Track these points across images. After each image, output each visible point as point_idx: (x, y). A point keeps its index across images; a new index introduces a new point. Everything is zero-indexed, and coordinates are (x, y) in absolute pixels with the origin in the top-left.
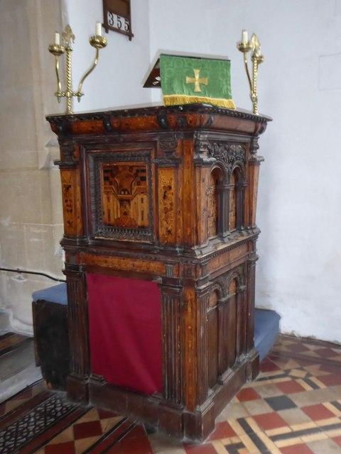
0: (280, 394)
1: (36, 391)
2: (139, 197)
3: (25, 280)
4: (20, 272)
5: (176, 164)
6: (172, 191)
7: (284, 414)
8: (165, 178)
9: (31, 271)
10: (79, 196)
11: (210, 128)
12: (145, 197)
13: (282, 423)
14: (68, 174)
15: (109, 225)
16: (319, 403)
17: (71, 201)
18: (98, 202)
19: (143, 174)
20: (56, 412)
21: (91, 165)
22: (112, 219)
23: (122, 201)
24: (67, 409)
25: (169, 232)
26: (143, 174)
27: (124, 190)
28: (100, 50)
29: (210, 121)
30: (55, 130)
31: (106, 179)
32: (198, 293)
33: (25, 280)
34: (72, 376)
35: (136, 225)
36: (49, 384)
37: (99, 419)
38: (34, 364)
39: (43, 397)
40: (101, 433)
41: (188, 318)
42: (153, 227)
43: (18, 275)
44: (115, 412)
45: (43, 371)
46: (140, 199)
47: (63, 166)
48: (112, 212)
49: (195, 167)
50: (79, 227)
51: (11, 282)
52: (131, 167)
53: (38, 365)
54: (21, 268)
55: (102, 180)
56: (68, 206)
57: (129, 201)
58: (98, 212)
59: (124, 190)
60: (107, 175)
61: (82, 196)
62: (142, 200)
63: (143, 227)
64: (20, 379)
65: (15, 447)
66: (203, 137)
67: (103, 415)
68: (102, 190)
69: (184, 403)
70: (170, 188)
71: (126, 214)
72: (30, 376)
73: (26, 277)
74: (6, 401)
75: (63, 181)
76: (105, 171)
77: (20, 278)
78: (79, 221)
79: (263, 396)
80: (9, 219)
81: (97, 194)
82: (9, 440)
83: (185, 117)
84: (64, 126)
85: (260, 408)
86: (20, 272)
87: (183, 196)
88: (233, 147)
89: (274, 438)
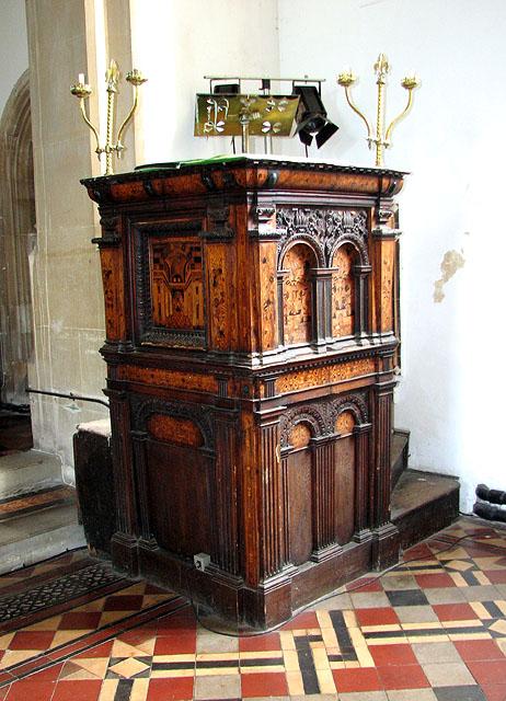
0: (414, 587)
1: (77, 556)
2: (194, 285)
3: (80, 410)
4: (72, 397)
5: (228, 241)
6: (223, 276)
7: (399, 611)
8: (215, 257)
9: (91, 397)
10: (122, 286)
11: (269, 185)
12: (201, 285)
13: (394, 619)
14: (108, 254)
15: (161, 325)
16: (465, 601)
17: (111, 291)
18: (146, 296)
19: (198, 254)
20: (93, 581)
21: (139, 243)
22: (164, 318)
23: (174, 291)
24: (108, 580)
25: (221, 333)
26: (198, 254)
27: (177, 276)
28: (348, 89)
29: (269, 179)
30: (94, 198)
31: (156, 261)
32: (258, 419)
33: (80, 410)
34: (116, 537)
35: (191, 324)
36: (94, 550)
37: (145, 596)
38: (77, 522)
39: (86, 564)
40: (139, 607)
41: (246, 456)
42: (203, 330)
43: (71, 403)
44: (168, 589)
45: (87, 530)
46: (194, 287)
47: (103, 244)
48: (163, 306)
49: (251, 243)
50: (123, 329)
51: (63, 412)
52: (184, 244)
53: (80, 523)
54: (75, 393)
55: (151, 261)
56: (109, 299)
57: (182, 291)
58: (147, 306)
59: (177, 276)
60: (157, 255)
61: (127, 286)
62: (197, 288)
63: (198, 327)
64: (57, 539)
65: (29, 611)
66: (266, 201)
67: (150, 590)
68: (151, 276)
69: (244, 577)
70: (220, 271)
71: (178, 310)
72: (66, 537)
73: (81, 405)
74: (36, 564)
75: (103, 265)
76: (155, 251)
77: (73, 408)
78: (122, 318)
79: (387, 588)
80: (60, 323)
81: (146, 284)
82: (25, 603)
83: (233, 176)
84: (100, 189)
85: (367, 601)
86: (72, 397)
87: (237, 282)
88: (334, 214)
89: (367, 635)
